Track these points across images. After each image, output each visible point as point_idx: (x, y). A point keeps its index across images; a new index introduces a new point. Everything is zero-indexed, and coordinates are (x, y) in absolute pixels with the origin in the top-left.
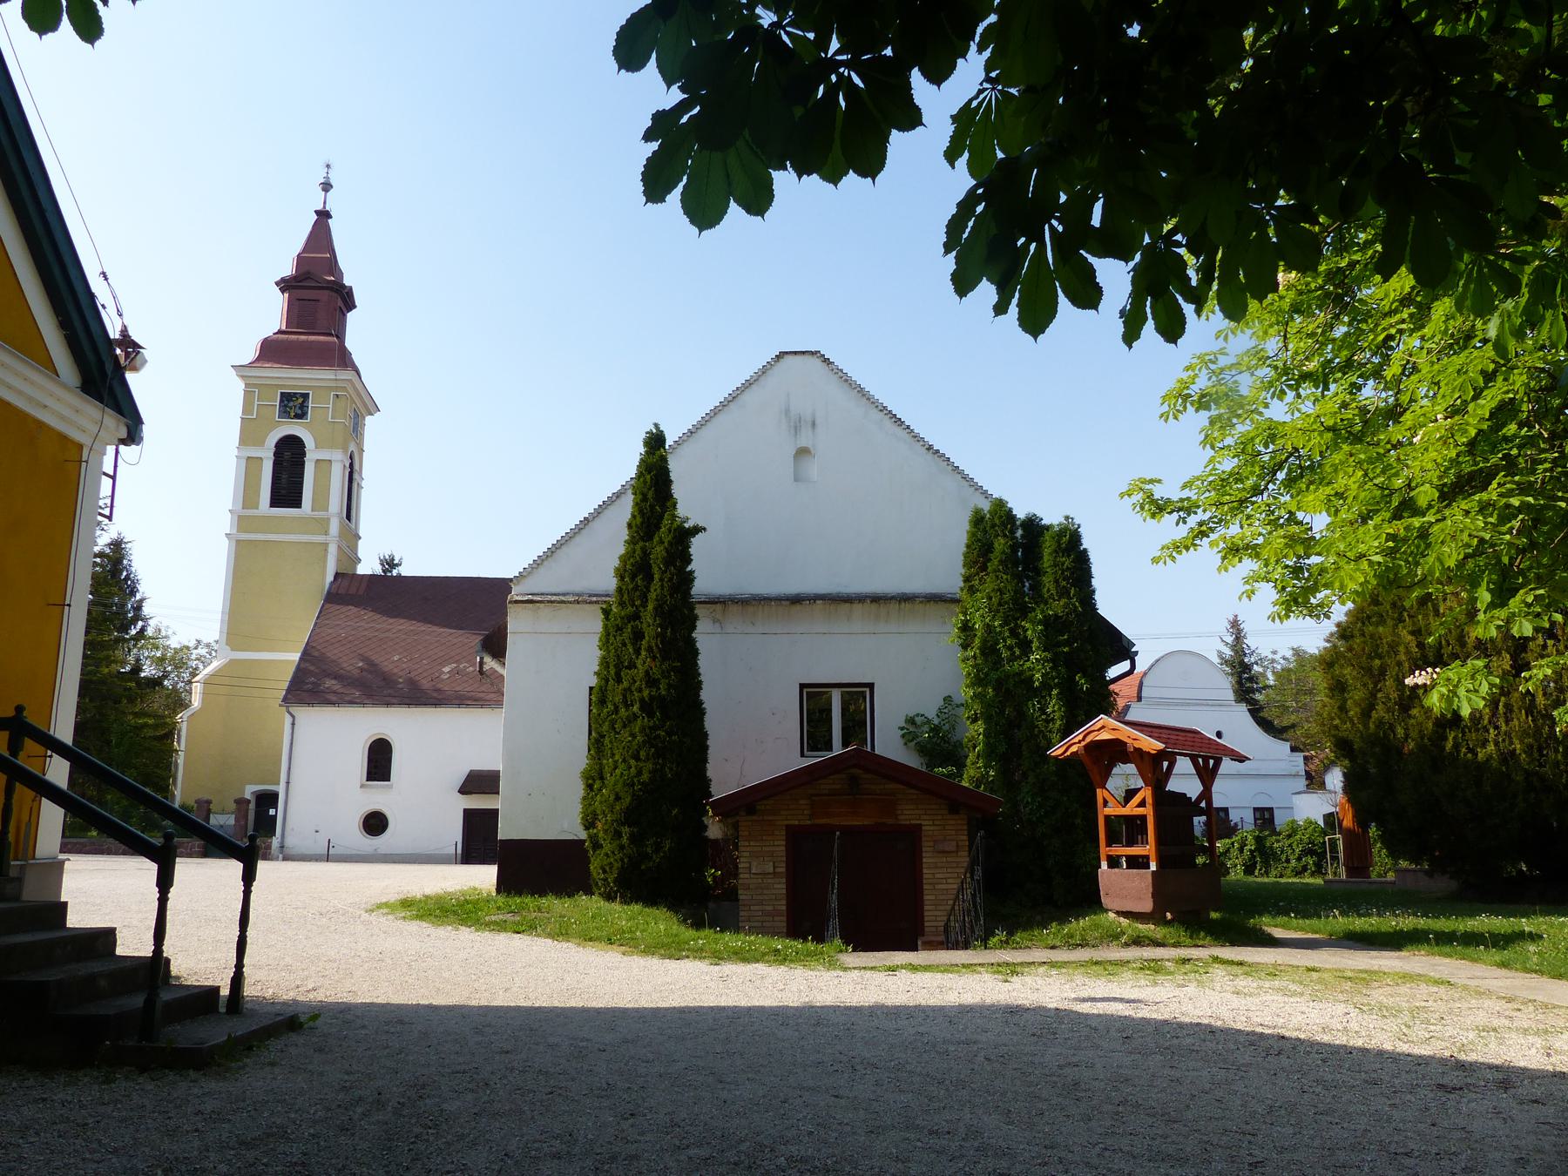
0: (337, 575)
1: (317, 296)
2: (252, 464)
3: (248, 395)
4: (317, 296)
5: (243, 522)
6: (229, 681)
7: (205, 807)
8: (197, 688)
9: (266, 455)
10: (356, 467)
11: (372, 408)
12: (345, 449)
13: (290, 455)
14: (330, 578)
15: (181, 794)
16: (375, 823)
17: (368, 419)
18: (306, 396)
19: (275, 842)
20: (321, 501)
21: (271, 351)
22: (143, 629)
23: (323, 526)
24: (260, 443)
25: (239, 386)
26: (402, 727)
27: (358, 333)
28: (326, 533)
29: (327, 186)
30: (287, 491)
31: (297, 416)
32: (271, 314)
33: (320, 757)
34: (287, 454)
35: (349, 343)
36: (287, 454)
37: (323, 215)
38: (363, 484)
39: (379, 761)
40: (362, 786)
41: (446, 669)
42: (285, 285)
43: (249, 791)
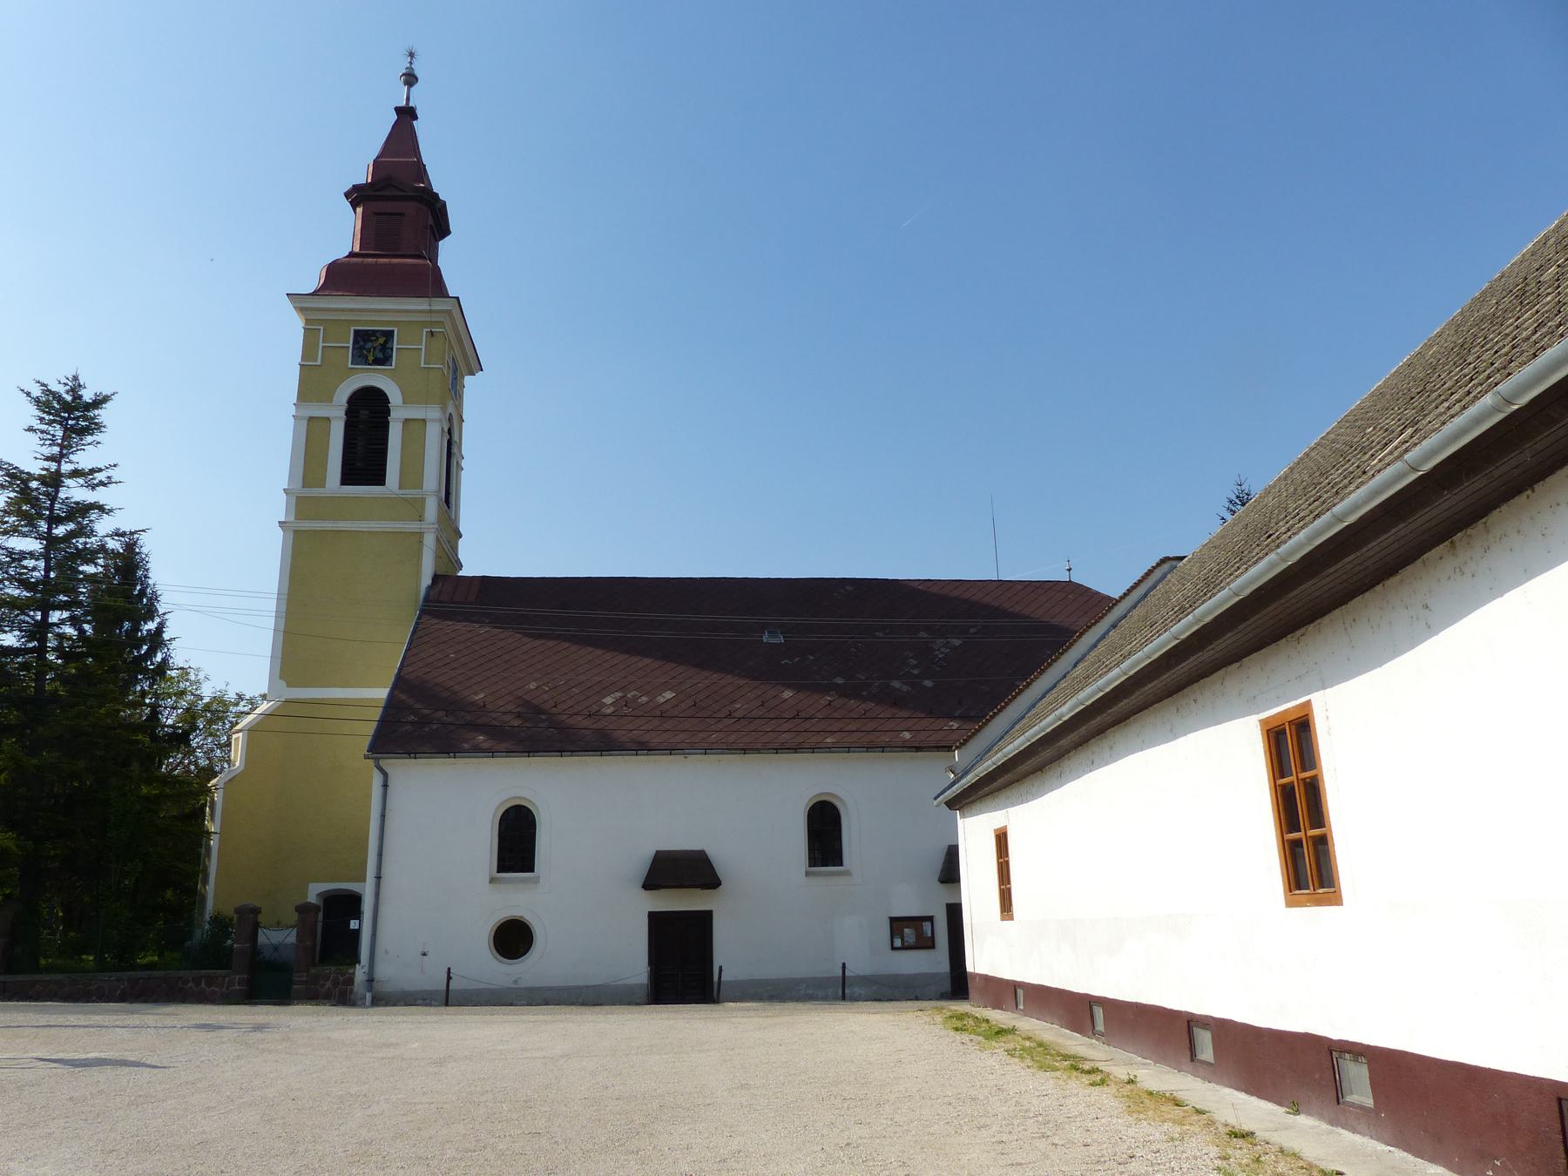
0: (436, 578)
1: (400, 212)
2: (313, 431)
3: (310, 335)
4: (400, 212)
5: (304, 504)
6: (287, 723)
7: (250, 918)
8: (238, 740)
9: (336, 413)
10: (456, 438)
11: (475, 366)
12: (444, 409)
13: (368, 415)
14: (426, 580)
15: (216, 893)
16: (513, 938)
17: (468, 380)
18: (389, 334)
19: (360, 973)
20: (412, 475)
21: (339, 277)
22: (165, 660)
23: (415, 508)
24: (328, 398)
25: (293, 328)
26: (556, 788)
27: (453, 258)
28: (421, 519)
29: (410, 79)
30: (364, 463)
31: (377, 362)
32: (340, 234)
33: (429, 832)
34: (364, 414)
35: (444, 262)
36: (364, 414)
37: (406, 114)
38: (464, 463)
39: (517, 841)
40: (492, 880)
41: (609, 700)
42: (357, 196)
43: (314, 892)
